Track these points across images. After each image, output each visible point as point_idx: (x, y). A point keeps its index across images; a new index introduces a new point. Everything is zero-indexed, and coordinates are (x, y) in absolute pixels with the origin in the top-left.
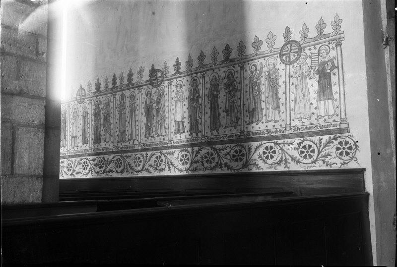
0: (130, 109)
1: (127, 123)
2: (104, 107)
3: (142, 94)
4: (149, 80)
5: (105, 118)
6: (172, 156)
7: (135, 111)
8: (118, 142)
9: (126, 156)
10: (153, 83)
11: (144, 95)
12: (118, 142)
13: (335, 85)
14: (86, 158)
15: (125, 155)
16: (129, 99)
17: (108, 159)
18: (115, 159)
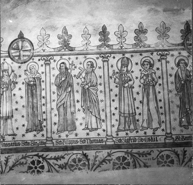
0: (142, 81)
1: (137, 104)
2: (80, 74)
3: (167, 62)
4: (183, 44)
5: (85, 92)
6: (149, 157)
7: (154, 86)
8: (27, 131)
9: (139, 154)
10: (189, 49)
11: (172, 64)
12: (27, 131)
13: (172, 83)
14: (37, 155)
15: (135, 151)
16: (139, 67)
17: (96, 157)
18: (114, 157)
